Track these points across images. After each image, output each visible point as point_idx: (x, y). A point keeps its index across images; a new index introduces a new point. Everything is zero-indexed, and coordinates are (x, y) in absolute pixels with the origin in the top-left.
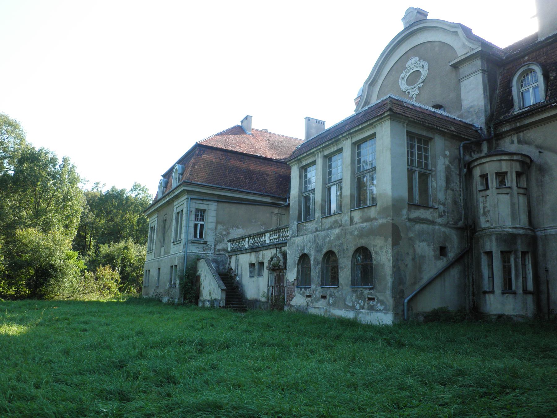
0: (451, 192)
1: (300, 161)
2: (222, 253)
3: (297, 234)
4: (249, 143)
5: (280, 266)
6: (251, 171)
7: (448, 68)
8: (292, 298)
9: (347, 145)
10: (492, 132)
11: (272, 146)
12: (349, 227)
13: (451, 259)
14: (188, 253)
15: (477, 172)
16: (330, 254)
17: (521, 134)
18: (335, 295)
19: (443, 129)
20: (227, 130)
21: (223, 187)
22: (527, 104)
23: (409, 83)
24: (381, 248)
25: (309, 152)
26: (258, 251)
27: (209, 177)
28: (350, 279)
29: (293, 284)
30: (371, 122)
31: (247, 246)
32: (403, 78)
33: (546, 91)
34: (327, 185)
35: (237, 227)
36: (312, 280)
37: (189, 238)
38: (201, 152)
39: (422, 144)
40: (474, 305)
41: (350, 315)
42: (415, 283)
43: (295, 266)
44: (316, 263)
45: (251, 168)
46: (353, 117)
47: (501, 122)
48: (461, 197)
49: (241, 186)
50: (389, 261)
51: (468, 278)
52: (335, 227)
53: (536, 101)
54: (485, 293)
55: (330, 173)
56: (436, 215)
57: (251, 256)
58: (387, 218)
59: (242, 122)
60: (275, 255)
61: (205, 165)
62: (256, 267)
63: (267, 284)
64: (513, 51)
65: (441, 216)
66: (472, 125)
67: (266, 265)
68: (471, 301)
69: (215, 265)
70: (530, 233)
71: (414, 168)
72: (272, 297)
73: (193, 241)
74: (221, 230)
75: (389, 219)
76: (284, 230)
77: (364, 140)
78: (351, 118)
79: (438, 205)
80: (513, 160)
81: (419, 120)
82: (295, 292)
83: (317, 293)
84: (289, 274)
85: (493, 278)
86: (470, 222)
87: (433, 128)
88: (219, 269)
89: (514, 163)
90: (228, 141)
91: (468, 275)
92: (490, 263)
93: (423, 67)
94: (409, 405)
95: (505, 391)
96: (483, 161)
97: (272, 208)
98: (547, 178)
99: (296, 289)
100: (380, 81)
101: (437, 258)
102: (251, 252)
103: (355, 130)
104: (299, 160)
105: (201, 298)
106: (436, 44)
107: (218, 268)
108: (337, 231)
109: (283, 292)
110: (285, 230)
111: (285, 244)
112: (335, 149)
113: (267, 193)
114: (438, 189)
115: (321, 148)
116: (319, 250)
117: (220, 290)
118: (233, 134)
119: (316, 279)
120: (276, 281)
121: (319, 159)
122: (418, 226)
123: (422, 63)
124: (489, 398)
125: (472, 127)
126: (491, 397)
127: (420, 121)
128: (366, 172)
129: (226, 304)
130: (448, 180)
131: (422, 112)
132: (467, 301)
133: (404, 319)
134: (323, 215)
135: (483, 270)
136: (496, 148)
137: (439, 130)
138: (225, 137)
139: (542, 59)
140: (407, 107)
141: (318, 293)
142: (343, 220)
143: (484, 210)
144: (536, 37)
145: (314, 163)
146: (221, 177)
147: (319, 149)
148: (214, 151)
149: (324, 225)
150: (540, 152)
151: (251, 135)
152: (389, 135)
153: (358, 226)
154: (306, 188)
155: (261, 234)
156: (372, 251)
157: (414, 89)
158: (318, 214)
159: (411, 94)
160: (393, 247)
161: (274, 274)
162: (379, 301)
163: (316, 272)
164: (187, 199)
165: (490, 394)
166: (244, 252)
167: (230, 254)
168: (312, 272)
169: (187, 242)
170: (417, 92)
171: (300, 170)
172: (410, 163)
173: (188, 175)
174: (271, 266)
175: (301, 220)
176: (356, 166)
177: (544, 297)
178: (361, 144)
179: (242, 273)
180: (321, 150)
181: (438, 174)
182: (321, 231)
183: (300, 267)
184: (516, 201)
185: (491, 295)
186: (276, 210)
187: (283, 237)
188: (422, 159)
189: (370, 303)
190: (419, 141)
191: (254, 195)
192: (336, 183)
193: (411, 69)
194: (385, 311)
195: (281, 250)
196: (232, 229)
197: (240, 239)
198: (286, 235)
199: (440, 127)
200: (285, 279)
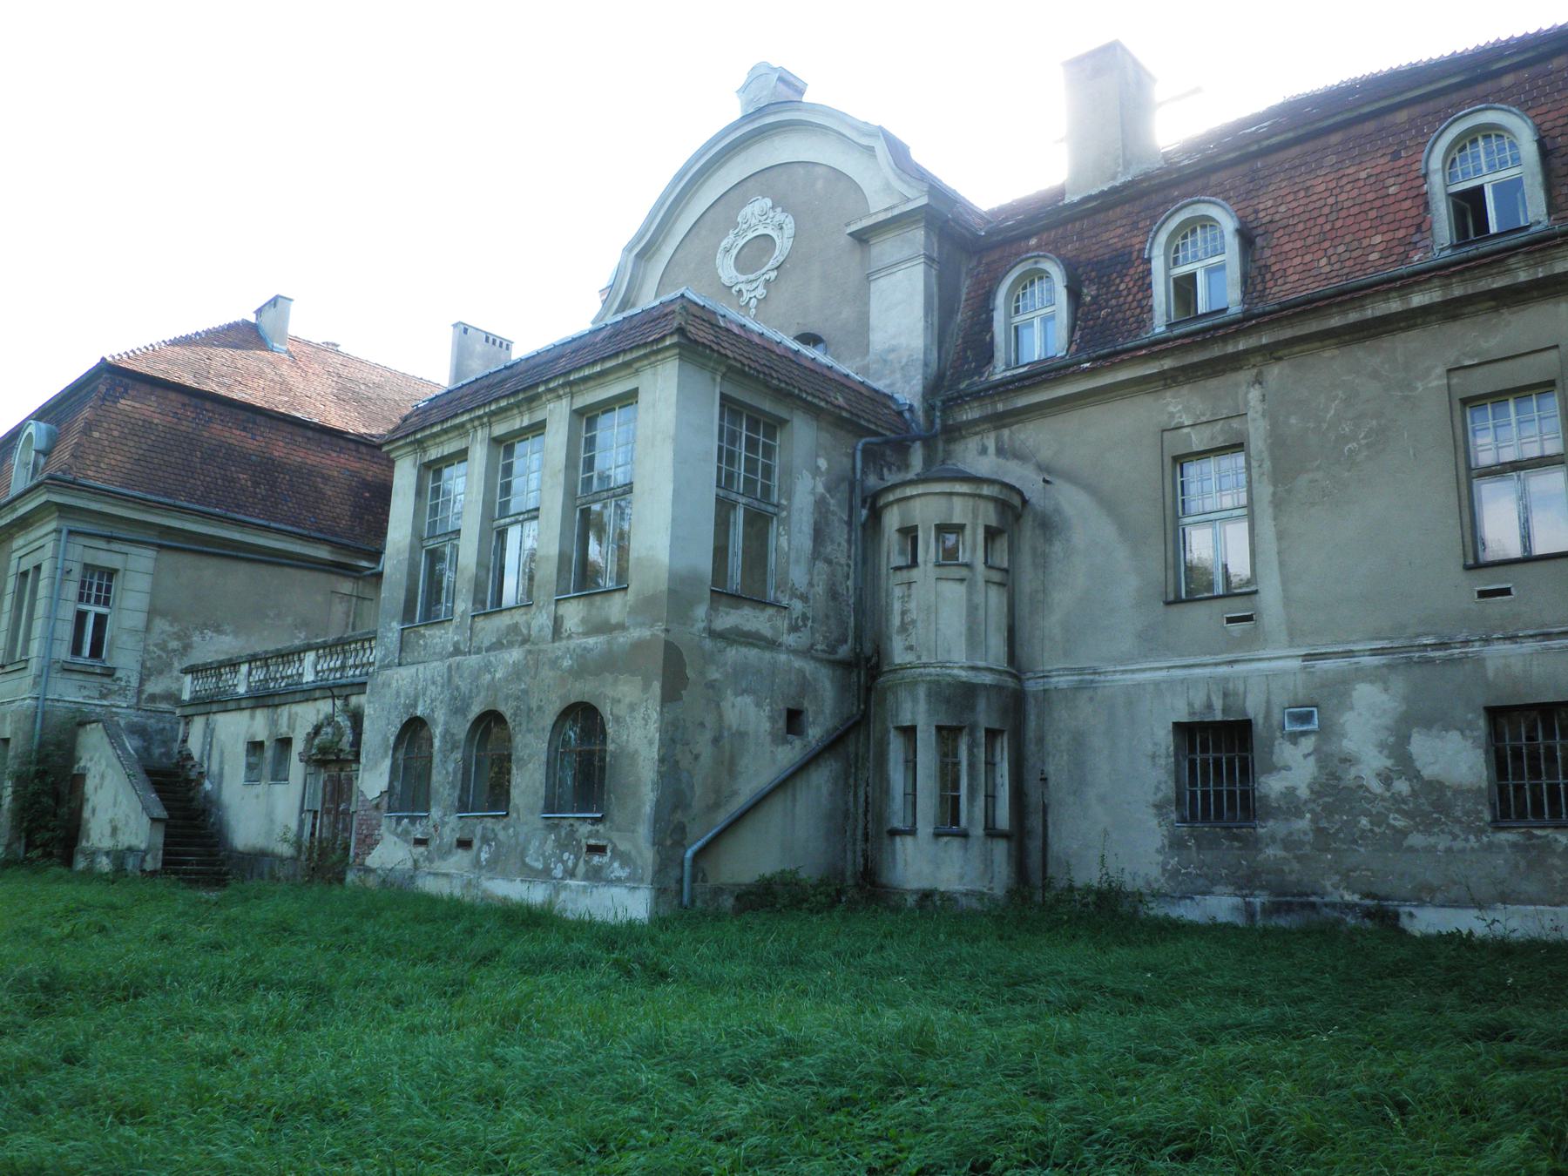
0: (825, 566)
1: (420, 445)
2: (164, 706)
3: (400, 659)
4: (277, 378)
5: (341, 750)
6: (273, 464)
7: (844, 240)
8: (371, 847)
9: (557, 414)
10: (938, 421)
11: (347, 394)
12: (548, 647)
13: (814, 743)
14: (49, 703)
15: (892, 520)
16: (490, 723)
17: (1006, 432)
18: (495, 838)
19: (816, 401)
20: (208, 332)
21: (178, 503)
22: (1025, 359)
23: (742, 264)
24: (632, 707)
25: (449, 424)
26: (277, 706)
27: (136, 467)
28: (542, 792)
29: (377, 807)
30: (628, 357)
31: (242, 689)
32: (727, 251)
33: (1072, 330)
34: (496, 523)
35: (218, 630)
36: (433, 796)
37: (55, 656)
38: (114, 390)
39: (758, 434)
40: (866, 865)
41: (536, 895)
42: (715, 806)
43: (386, 752)
44: (449, 746)
45: (276, 454)
46: (581, 337)
47: (960, 397)
48: (850, 583)
49: (238, 506)
50: (651, 743)
51: (856, 794)
52: (511, 644)
53: (1046, 353)
54: (894, 833)
55: (507, 489)
56: (784, 625)
57: (252, 717)
58: (652, 626)
59: (259, 312)
60: (330, 720)
61: (126, 431)
62: (269, 754)
63: (297, 804)
64: (1006, 219)
65: (794, 628)
66: (891, 398)
67: (298, 746)
68: (859, 854)
69: (137, 742)
70: (1010, 682)
71: (733, 496)
72: (312, 843)
73: (66, 666)
74: (164, 636)
75: (658, 630)
76: (359, 644)
77: (607, 406)
78: (574, 340)
79: (791, 599)
80: (980, 496)
81: (755, 369)
82: (383, 828)
83: (447, 831)
84: (366, 776)
85: (915, 795)
86: (868, 648)
87: (790, 395)
88: (150, 755)
89: (982, 504)
90: (209, 366)
91: (856, 786)
92: (911, 757)
93: (781, 228)
94: (633, 1142)
95: (892, 1092)
96: (909, 491)
97: (333, 578)
98: (1057, 548)
99: (385, 822)
100: (668, 251)
101: (778, 740)
102: (253, 708)
103: (582, 374)
104: (420, 442)
105: (84, 843)
106: (819, 170)
107: (144, 754)
108: (515, 655)
109: (347, 829)
110: (363, 646)
111: (360, 687)
112: (526, 423)
113: (321, 531)
114: (793, 555)
115: (485, 414)
116: (458, 709)
117: (145, 820)
118: (226, 346)
119: (446, 792)
120: (327, 797)
121: (478, 446)
122: (734, 651)
123: (780, 216)
124: (849, 1114)
125: (890, 403)
126: (856, 1110)
127: (758, 372)
128: (605, 494)
129: (165, 863)
130: (819, 534)
131: (764, 348)
132: (849, 856)
133: (681, 904)
134: (479, 607)
135: (892, 773)
136: (943, 462)
137: (805, 400)
138: (201, 351)
139: (1069, 249)
140: (728, 330)
141: (449, 834)
142: (535, 625)
143: (903, 619)
144: (1061, 193)
145: (461, 456)
146: (176, 471)
147: (479, 417)
148: (159, 392)
149: (480, 636)
150: (1045, 481)
151: (286, 356)
152: (673, 399)
153: (573, 643)
154: (433, 525)
155: (288, 655)
156: (608, 716)
157: (755, 285)
158: (463, 605)
159: (746, 296)
160: (662, 706)
161: (323, 776)
162: (616, 854)
163: (447, 773)
164: (58, 531)
165: (855, 1102)
166: (231, 705)
167: (188, 711)
168: (434, 772)
169: (49, 667)
170: (761, 292)
171: (419, 471)
172: (725, 480)
173: (66, 456)
174: (314, 751)
175: (412, 620)
176: (581, 476)
177: (1034, 845)
178: (597, 416)
179: (221, 769)
180: (485, 420)
181: (795, 517)
182: (470, 652)
183: (401, 755)
184: (979, 599)
185: (909, 840)
186: (346, 586)
187: (356, 667)
188: (756, 475)
189: (591, 859)
190: (753, 425)
191: (277, 536)
192: (521, 518)
193: (749, 227)
194: (632, 882)
195: (347, 705)
196: (202, 633)
197: (221, 664)
198: (365, 660)
199: (808, 394)
200: (354, 789)
